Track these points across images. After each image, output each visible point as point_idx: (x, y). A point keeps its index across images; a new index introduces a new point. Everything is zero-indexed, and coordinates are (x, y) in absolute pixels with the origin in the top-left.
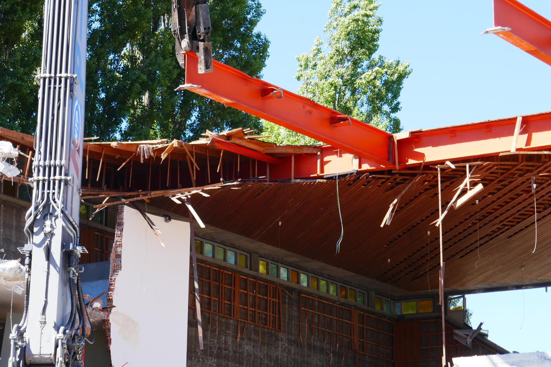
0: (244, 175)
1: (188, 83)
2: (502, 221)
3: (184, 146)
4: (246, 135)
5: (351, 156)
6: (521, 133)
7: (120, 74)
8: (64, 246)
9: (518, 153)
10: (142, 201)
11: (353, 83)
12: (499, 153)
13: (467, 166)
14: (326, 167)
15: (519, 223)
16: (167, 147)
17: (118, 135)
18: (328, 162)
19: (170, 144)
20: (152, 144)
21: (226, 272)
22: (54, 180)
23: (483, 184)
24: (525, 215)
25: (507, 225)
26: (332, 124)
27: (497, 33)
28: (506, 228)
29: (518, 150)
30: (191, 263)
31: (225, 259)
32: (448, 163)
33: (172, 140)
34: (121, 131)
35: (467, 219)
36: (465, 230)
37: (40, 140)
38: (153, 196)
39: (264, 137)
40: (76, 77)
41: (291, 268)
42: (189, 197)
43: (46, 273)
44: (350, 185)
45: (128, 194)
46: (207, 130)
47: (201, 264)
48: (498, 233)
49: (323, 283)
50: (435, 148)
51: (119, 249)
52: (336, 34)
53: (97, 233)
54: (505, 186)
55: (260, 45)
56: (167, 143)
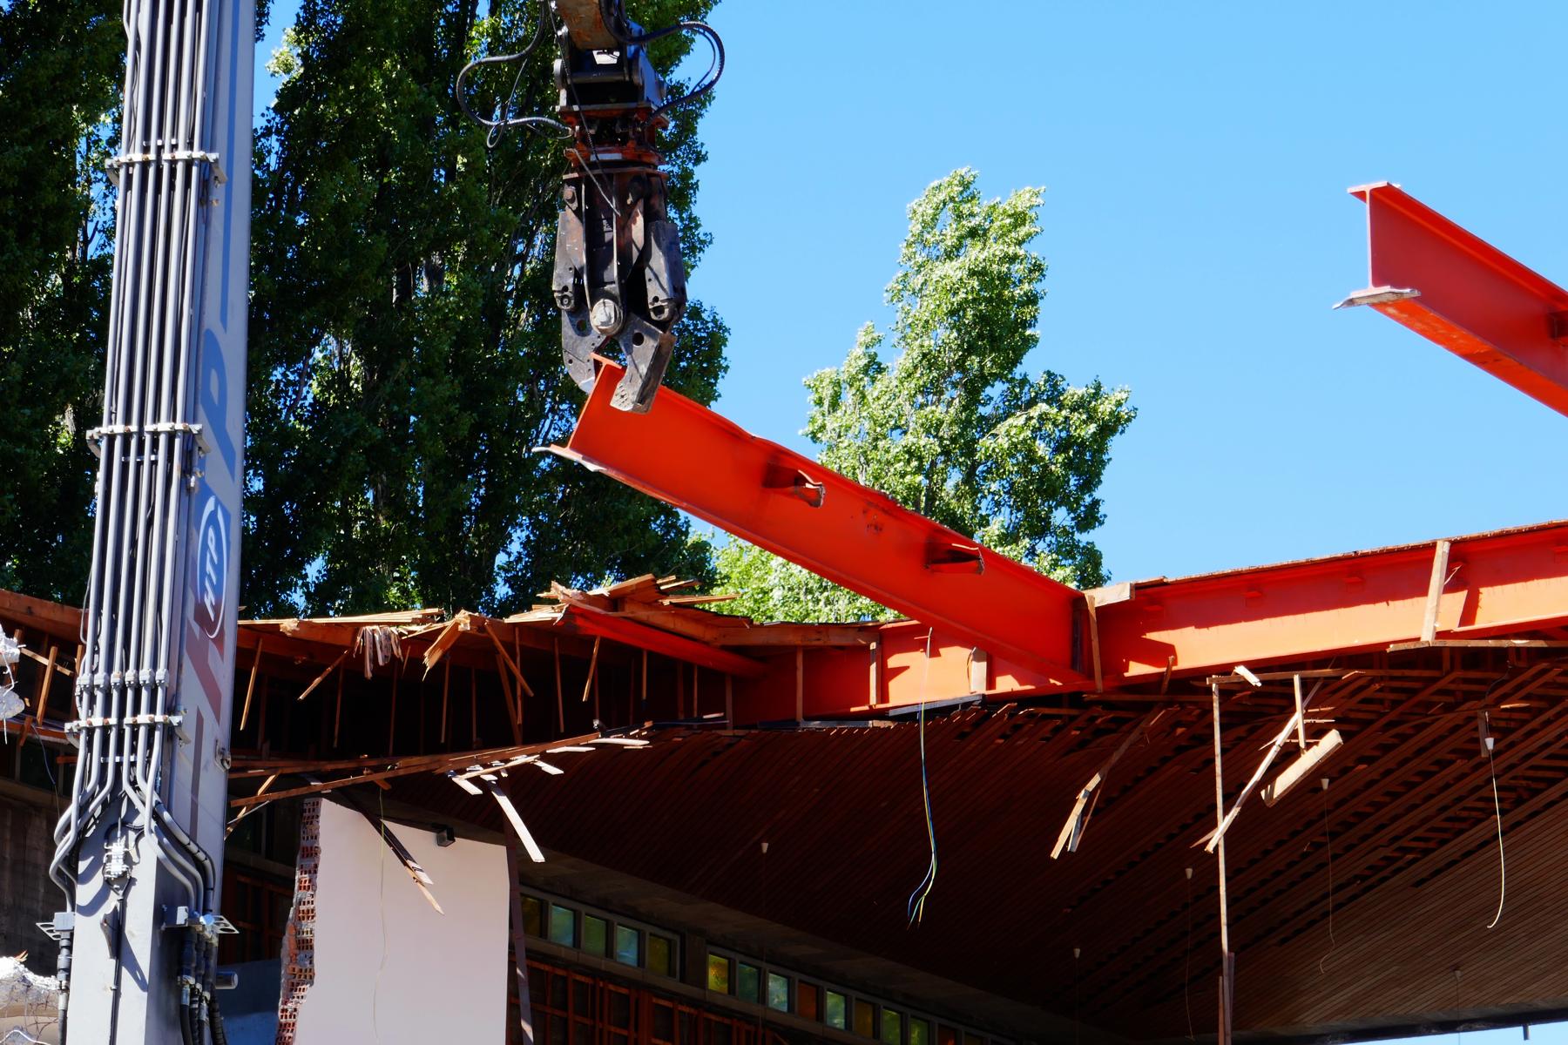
0: (659, 712)
1: (573, 448)
2: (1396, 839)
3: (489, 630)
4: (666, 594)
5: (965, 652)
6: (1449, 589)
7: (306, 423)
8: (162, 914)
9: (1440, 643)
10: (371, 787)
11: (969, 449)
12: (1387, 644)
13: (1296, 679)
14: (894, 685)
15: (1443, 842)
16: (440, 631)
17: (298, 598)
18: (899, 671)
19: (449, 624)
20: (397, 624)
21: (611, 987)
22: (135, 727)
23: (1342, 734)
24: (1464, 820)
25: (1411, 850)
26: (918, 557)
27: (1380, 305)
28: (1410, 857)
29: (1440, 635)
30: (512, 965)
31: (609, 951)
32: (1242, 671)
33: (456, 611)
34: (306, 585)
35: (1296, 833)
36: (1291, 865)
37: (98, 614)
38: (401, 772)
39: (719, 599)
40: (200, 432)
41: (797, 976)
42: (504, 775)
43: (111, 993)
44: (963, 736)
45: (330, 767)
46: (554, 583)
47: (542, 967)
48: (1385, 873)
49: (890, 1016)
50: (1204, 630)
51: (307, 925)
52: (921, 309)
53: (242, 879)
54: (1404, 738)
55: (699, 339)
56: (442, 620)
